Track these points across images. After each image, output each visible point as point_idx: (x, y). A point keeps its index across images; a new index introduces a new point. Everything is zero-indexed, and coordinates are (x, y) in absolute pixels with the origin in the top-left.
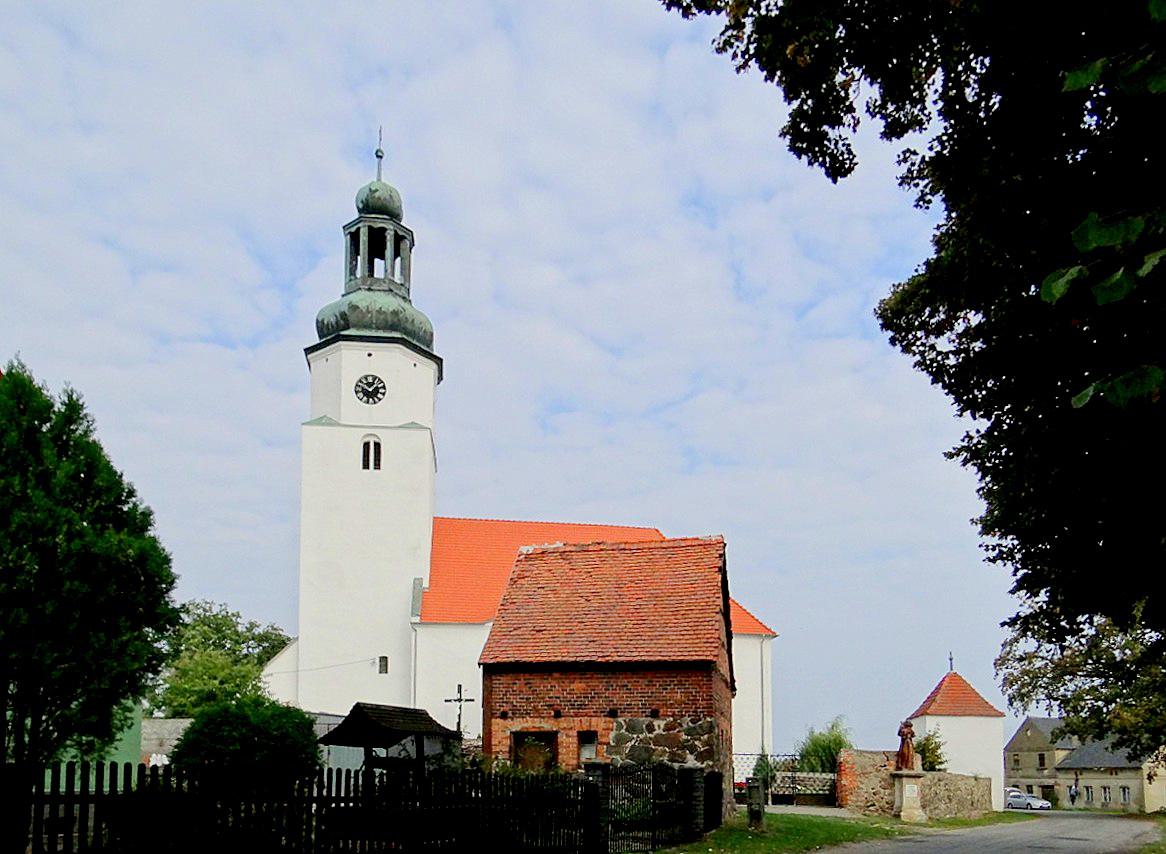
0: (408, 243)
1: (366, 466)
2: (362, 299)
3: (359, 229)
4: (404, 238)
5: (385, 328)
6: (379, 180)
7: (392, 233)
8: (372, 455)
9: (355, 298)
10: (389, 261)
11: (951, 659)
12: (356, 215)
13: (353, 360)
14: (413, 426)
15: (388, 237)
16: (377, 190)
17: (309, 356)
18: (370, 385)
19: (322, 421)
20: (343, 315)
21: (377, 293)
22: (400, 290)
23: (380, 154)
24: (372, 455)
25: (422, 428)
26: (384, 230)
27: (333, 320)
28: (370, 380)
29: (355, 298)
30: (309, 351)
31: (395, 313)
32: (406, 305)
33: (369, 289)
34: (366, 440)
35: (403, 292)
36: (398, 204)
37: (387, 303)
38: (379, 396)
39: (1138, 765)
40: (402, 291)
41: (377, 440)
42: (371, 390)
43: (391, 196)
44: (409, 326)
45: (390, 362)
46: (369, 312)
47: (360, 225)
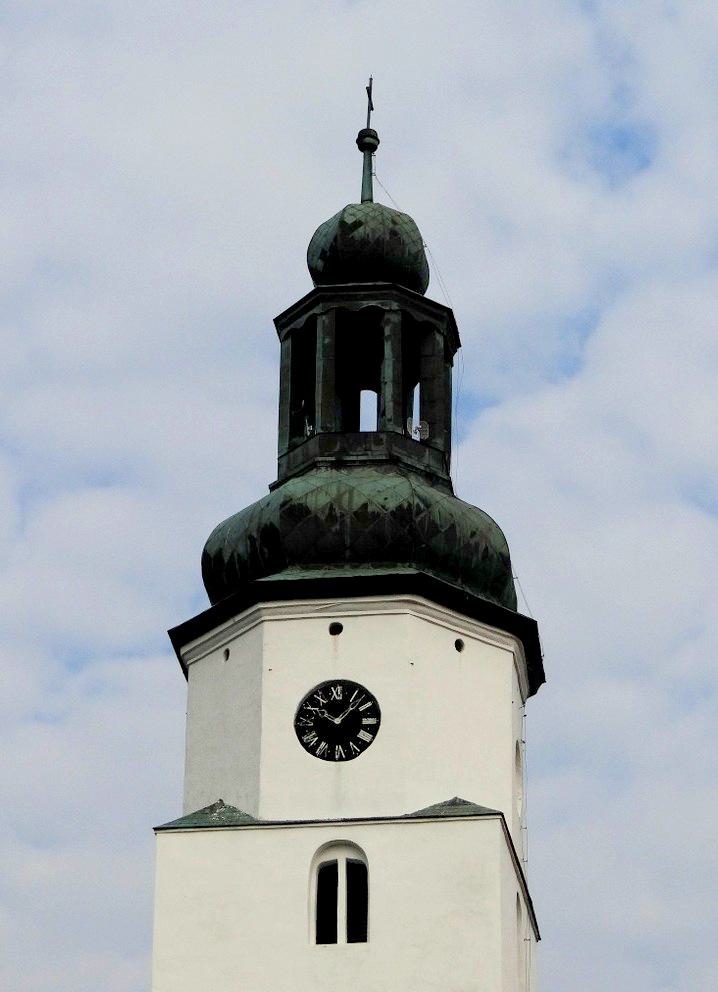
0: (440, 339)
1: (326, 935)
2: (318, 488)
3: (312, 320)
4: (429, 329)
5: (378, 559)
6: (367, 198)
7: (395, 318)
8: (342, 902)
9: (296, 487)
10: (388, 390)
11: (367, 142)
12: (308, 286)
13: (298, 646)
14: (456, 810)
15: (387, 331)
16: (357, 224)
17: (183, 651)
18: (335, 708)
19: (204, 820)
20: (268, 533)
21: (358, 472)
22: (420, 457)
23: (368, 140)
24: (342, 902)
25: (479, 813)
26: (378, 313)
27: (242, 549)
28: (337, 694)
29: (296, 487)
30: (182, 636)
31: (403, 514)
32: (434, 494)
33: (339, 465)
34: (328, 857)
35: (428, 460)
36: (414, 250)
37: (381, 489)
38: (363, 735)
39: (283, 509)
40: (432, 458)
41: (353, 856)
42: (338, 721)
43: (394, 233)
44: (439, 543)
45: (393, 645)
46: (332, 517)
47: (317, 310)
